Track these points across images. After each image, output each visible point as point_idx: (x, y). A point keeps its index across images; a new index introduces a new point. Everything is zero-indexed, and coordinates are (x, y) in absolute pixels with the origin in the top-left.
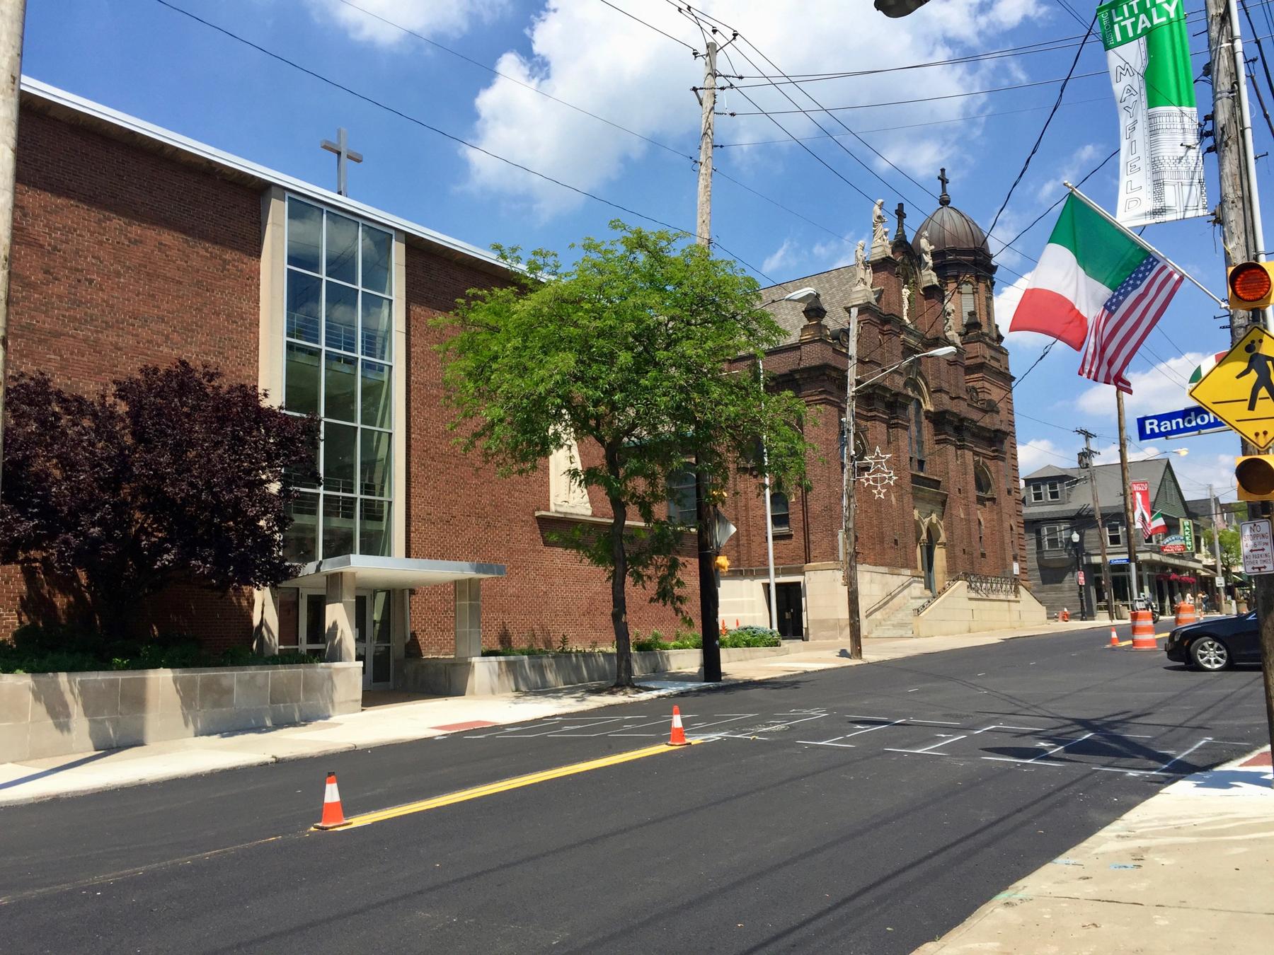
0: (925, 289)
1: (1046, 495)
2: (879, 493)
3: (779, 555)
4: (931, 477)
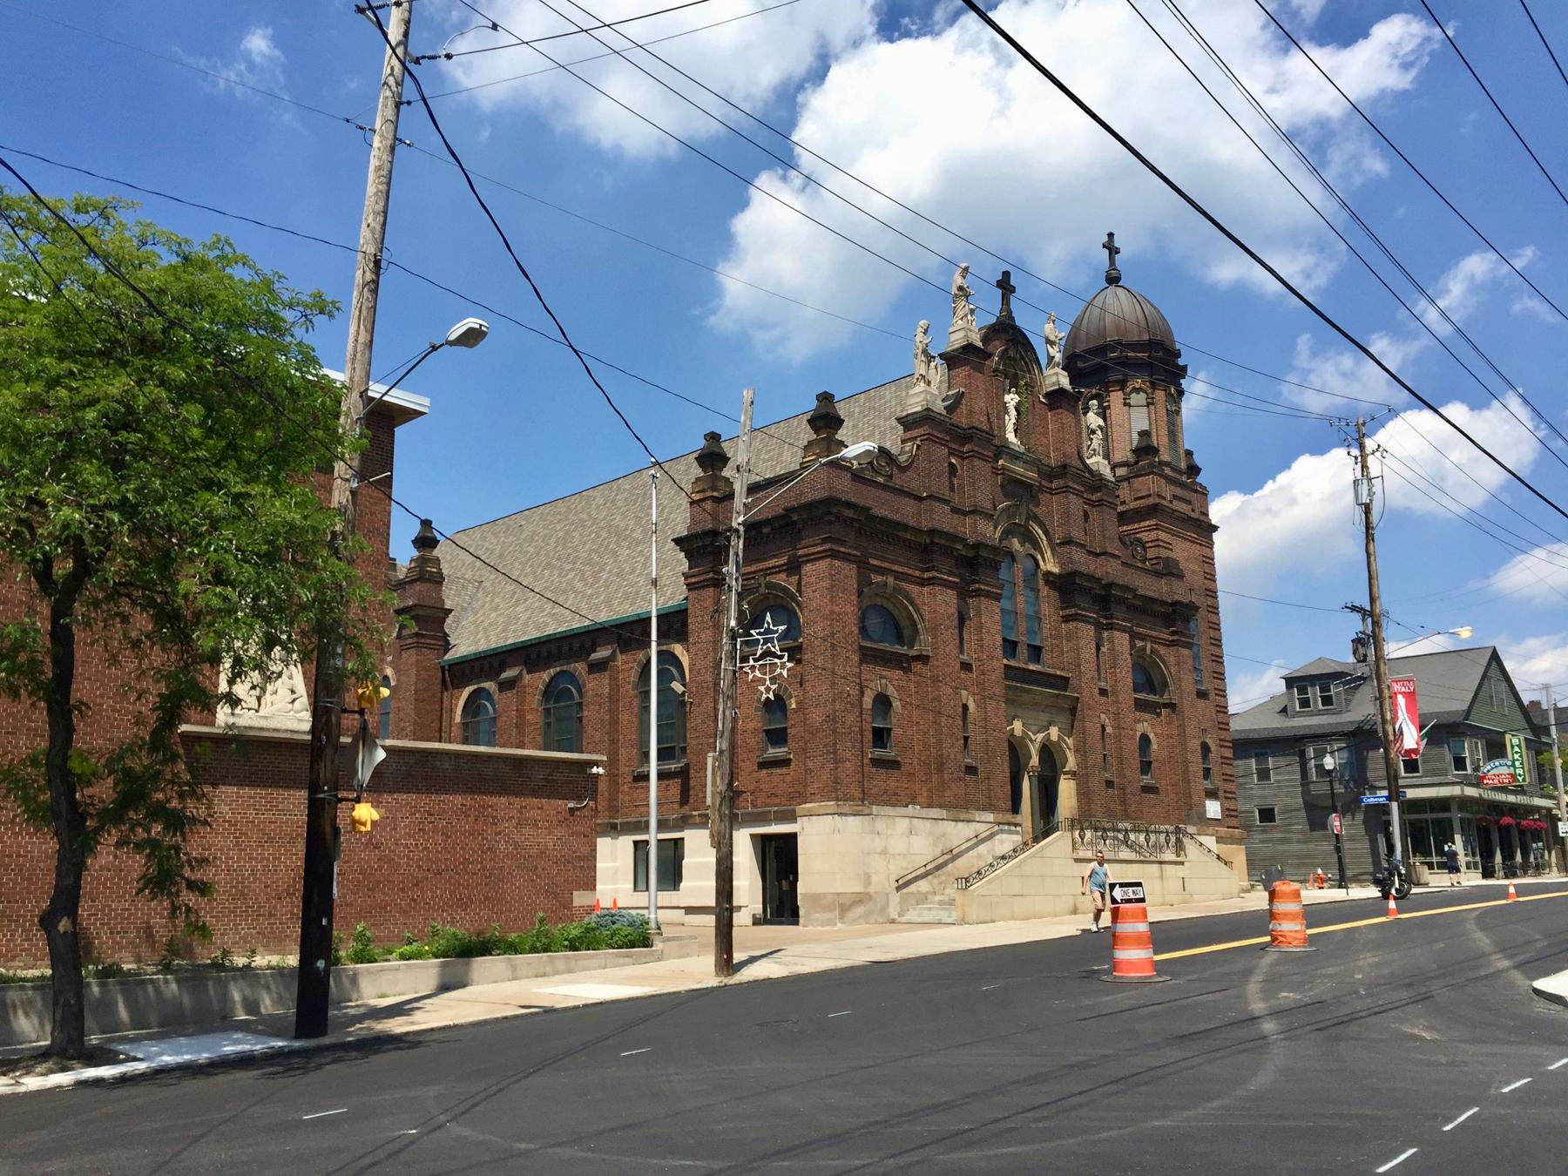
0: (1048, 395)
1: (1316, 701)
2: (768, 690)
3: (773, 791)
4: (1051, 671)
